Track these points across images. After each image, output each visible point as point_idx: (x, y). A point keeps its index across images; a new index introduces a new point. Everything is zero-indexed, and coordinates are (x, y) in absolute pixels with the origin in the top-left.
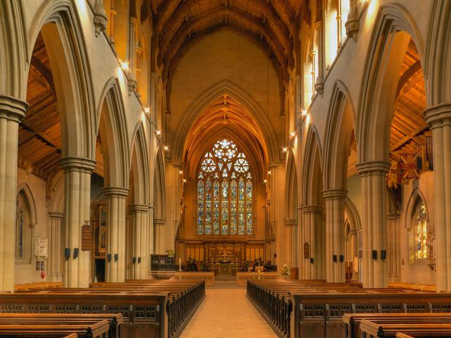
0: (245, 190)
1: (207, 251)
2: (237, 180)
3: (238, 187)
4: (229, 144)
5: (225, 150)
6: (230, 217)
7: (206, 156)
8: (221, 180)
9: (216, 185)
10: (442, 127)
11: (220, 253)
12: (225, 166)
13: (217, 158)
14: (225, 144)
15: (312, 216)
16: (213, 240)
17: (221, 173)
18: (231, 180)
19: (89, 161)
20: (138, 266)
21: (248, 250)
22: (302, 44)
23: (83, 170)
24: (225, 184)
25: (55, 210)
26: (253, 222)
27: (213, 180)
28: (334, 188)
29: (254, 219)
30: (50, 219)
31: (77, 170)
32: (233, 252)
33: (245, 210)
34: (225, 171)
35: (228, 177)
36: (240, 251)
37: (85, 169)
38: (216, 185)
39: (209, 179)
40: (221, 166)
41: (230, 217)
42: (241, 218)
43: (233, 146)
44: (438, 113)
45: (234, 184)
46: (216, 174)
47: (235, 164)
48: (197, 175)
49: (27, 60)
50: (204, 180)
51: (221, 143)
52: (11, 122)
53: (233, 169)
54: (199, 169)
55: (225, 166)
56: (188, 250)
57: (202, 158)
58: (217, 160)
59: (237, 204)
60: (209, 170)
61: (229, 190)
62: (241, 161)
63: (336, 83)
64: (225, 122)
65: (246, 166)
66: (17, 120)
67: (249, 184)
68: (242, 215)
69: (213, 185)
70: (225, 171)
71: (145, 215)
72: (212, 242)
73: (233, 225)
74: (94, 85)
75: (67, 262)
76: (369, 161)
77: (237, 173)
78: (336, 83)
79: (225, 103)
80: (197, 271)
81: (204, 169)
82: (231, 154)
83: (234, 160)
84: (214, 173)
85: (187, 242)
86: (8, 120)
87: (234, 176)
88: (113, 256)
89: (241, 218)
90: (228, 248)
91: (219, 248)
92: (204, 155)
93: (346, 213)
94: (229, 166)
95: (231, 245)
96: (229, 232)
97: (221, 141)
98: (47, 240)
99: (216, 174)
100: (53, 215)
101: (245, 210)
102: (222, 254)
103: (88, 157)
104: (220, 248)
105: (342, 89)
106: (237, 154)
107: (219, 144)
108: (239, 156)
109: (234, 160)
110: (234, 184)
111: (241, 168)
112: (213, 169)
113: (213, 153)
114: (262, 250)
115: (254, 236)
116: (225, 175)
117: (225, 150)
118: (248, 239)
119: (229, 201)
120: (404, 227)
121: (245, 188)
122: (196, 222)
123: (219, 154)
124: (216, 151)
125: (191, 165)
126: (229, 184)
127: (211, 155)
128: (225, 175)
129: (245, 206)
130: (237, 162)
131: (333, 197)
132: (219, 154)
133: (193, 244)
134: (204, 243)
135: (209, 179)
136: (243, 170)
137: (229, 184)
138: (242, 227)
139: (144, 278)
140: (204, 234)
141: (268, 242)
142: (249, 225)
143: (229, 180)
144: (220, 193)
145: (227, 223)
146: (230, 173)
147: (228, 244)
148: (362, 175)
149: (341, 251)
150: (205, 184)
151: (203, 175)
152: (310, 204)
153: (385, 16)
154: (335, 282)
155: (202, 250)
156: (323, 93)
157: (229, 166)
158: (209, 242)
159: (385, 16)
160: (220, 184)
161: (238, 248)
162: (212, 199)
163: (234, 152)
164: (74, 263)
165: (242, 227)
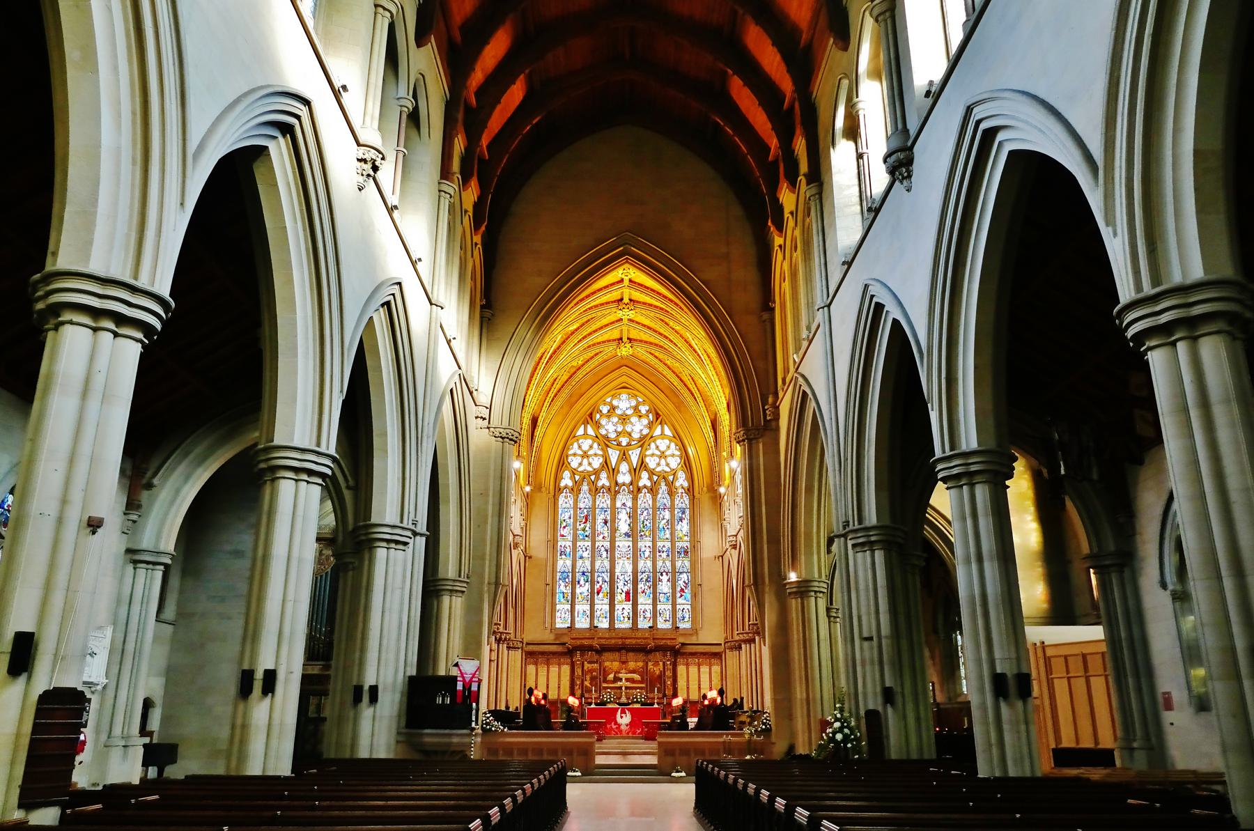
0: (672, 515)
1: (578, 671)
2: (653, 490)
3: (655, 509)
4: (634, 403)
5: (624, 419)
6: (635, 582)
7: (581, 431)
8: (614, 490)
9: (604, 501)
10: (1174, 344)
11: (611, 677)
12: (624, 457)
13: (606, 438)
14: (624, 403)
15: (879, 555)
16: (595, 643)
17: (614, 472)
18: (639, 490)
19: (403, 528)
20: (367, 712)
21: (681, 669)
22: (817, 110)
23: (305, 477)
24: (624, 499)
25: (146, 542)
26: (694, 595)
27: (595, 491)
28: (974, 445)
29: (696, 589)
30: (130, 568)
31: (384, 544)
32: (644, 672)
33: (673, 565)
34: (624, 467)
35: (631, 483)
36: (663, 673)
37: (120, 319)
38: (604, 501)
39: (585, 487)
40: (614, 455)
41: (635, 582)
42: (664, 587)
43: (643, 409)
44: (1158, 308)
45: (645, 499)
46: (604, 475)
47: (648, 453)
48: (557, 478)
49: (342, 391)
50: (575, 490)
51: (615, 403)
52: (119, 340)
53: (642, 464)
54: (562, 464)
55: (624, 457)
56: (531, 669)
57: (572, 436)
58: (605, 442)
59: (654, 549)
60: (585, 467)
61: (633, 516)
62: (663, 444)
63: (866, 286)
64: (625, 350)
65: (673, 455)
66: (140, 335)
67: (683, 501)
68: (665, 578)
69: (594, 501)
70: (624, 467)
71: (397, 555)
72: (590, 648)
73: (644, 602)
74: (183, 42)
75: (241, 706)
76: (964, 447)
77: (652, 473)
78: (866, 286)
79: (626, 300)
80: (549, 726)
81: (574, 464)
82: (638, 427)
83: (644, 441)
84: (597, 473)
85: (531, 648)
86: (116, 335)
87: (644, 480)
88: (259, 675)
89: (664, 587)
90: (632, 665)
91: (607, 664)
92: (575, 428)
93: (1069, 504)
94: (634, 456)
95: (641, 656)
96: (635, 622)
97: (613, 396)
98: (109, 632)
99: (604, 475)
100: (138, 557)
101: (673, 565)
102: (617, 679)
103: (318, 445)
104: (611, 662)
105: (882, 297)
106: (650, 426)
107: (610, 404)
108: (658, 431)
109: (644, 441)
110: (645, 499)
111: (663, 461)
112: (597, 463)
113: (598, 425)
114: (716, 669)
115: (694, 631)
116: (624, 478)
117: (624, 419)
118: (681, 640)
119: (635, 543)
120: (1157, 587)
121: (672, 509)
122: (553, 595)
123: (611, 428)
124: (603, 422)
125: (544, 455)
126: (635, 499)
127: (590, 431)
128: (624, 478)
129: (673, 553)
130: (653, 445)
131: (872, 543)
132: (610, 427)
133: (543, 653)
134: (570, 653)
135: (585, 487)
136: (668, 465)
137: (635, 499)
138: (664, 607)
139: (382, 754)
140: (571, 628)
141: (731, 649)
142: (684, 604)
143: (636, 491)
144: (611, 523)
145: (628, 599)
146: (635, 472)
147: (631, 654)
148: (792, 597)
149: (1018, 659)
150: (576, 502)
151: (573, 477)
152: (872, 518)
153: (978, 122)
154: (1012, 773)
155: (566, 669)
156: (909, 176)
157: (634, 456)
158: (584, 649)
159: (978, 122)
160: (614, 500)
161: (656, 664)
162: (593, 537)
163: (645, 421)
164: (260, 709)
165: (664, 607)
